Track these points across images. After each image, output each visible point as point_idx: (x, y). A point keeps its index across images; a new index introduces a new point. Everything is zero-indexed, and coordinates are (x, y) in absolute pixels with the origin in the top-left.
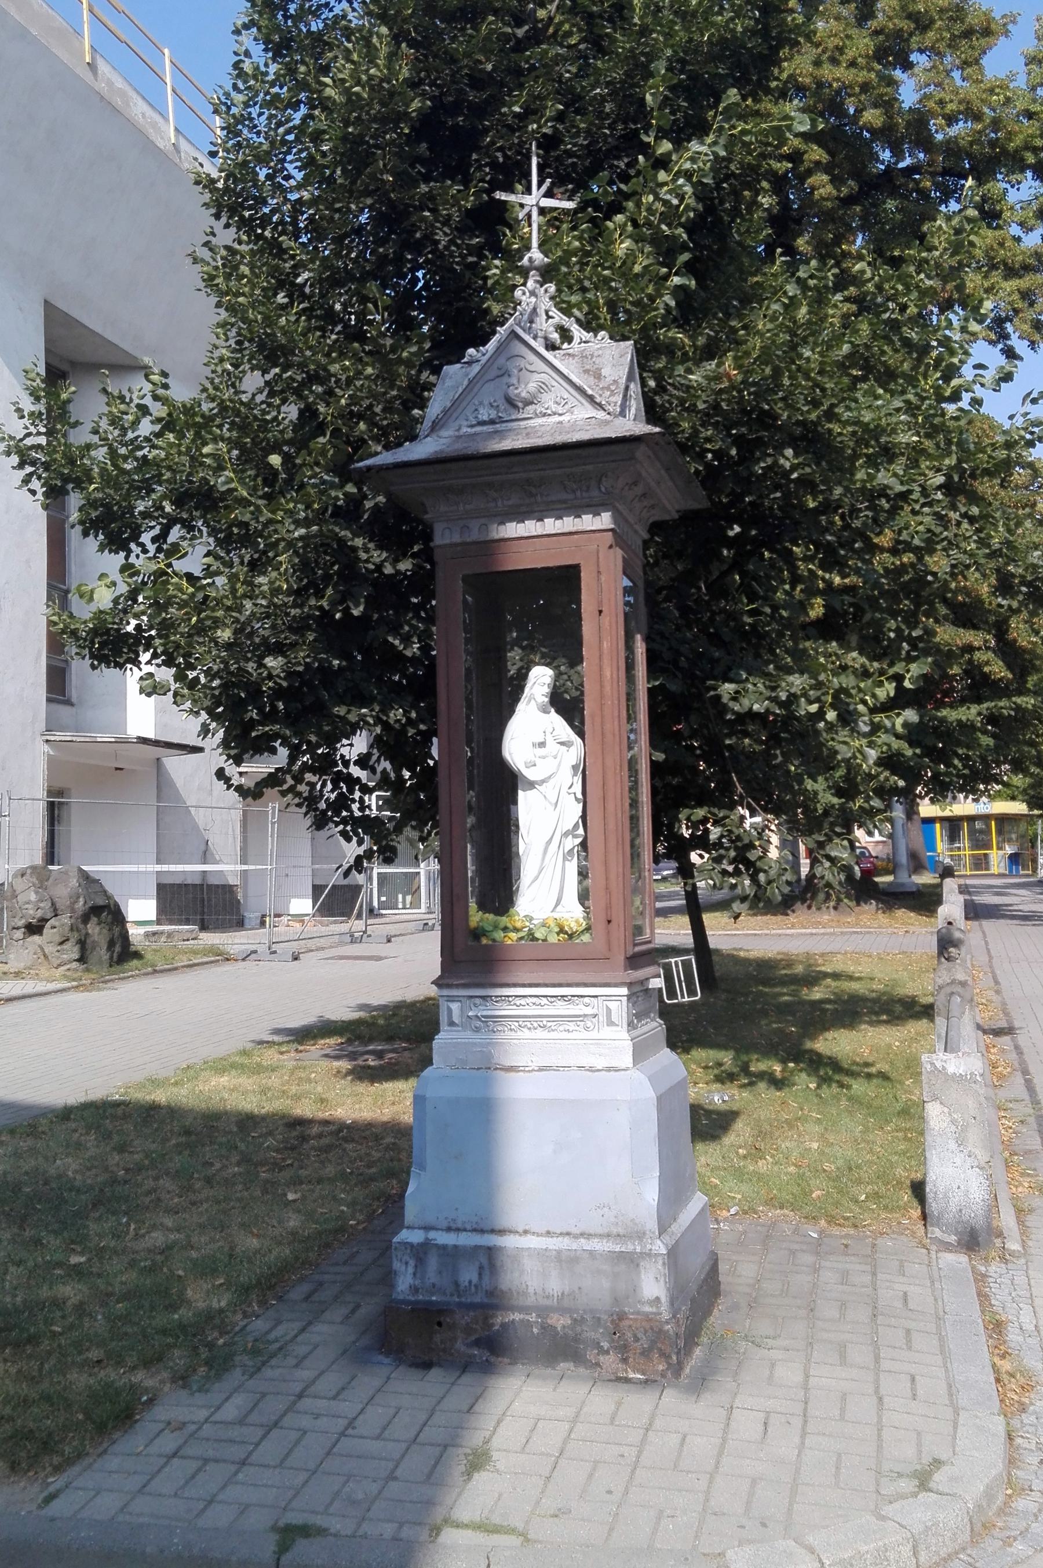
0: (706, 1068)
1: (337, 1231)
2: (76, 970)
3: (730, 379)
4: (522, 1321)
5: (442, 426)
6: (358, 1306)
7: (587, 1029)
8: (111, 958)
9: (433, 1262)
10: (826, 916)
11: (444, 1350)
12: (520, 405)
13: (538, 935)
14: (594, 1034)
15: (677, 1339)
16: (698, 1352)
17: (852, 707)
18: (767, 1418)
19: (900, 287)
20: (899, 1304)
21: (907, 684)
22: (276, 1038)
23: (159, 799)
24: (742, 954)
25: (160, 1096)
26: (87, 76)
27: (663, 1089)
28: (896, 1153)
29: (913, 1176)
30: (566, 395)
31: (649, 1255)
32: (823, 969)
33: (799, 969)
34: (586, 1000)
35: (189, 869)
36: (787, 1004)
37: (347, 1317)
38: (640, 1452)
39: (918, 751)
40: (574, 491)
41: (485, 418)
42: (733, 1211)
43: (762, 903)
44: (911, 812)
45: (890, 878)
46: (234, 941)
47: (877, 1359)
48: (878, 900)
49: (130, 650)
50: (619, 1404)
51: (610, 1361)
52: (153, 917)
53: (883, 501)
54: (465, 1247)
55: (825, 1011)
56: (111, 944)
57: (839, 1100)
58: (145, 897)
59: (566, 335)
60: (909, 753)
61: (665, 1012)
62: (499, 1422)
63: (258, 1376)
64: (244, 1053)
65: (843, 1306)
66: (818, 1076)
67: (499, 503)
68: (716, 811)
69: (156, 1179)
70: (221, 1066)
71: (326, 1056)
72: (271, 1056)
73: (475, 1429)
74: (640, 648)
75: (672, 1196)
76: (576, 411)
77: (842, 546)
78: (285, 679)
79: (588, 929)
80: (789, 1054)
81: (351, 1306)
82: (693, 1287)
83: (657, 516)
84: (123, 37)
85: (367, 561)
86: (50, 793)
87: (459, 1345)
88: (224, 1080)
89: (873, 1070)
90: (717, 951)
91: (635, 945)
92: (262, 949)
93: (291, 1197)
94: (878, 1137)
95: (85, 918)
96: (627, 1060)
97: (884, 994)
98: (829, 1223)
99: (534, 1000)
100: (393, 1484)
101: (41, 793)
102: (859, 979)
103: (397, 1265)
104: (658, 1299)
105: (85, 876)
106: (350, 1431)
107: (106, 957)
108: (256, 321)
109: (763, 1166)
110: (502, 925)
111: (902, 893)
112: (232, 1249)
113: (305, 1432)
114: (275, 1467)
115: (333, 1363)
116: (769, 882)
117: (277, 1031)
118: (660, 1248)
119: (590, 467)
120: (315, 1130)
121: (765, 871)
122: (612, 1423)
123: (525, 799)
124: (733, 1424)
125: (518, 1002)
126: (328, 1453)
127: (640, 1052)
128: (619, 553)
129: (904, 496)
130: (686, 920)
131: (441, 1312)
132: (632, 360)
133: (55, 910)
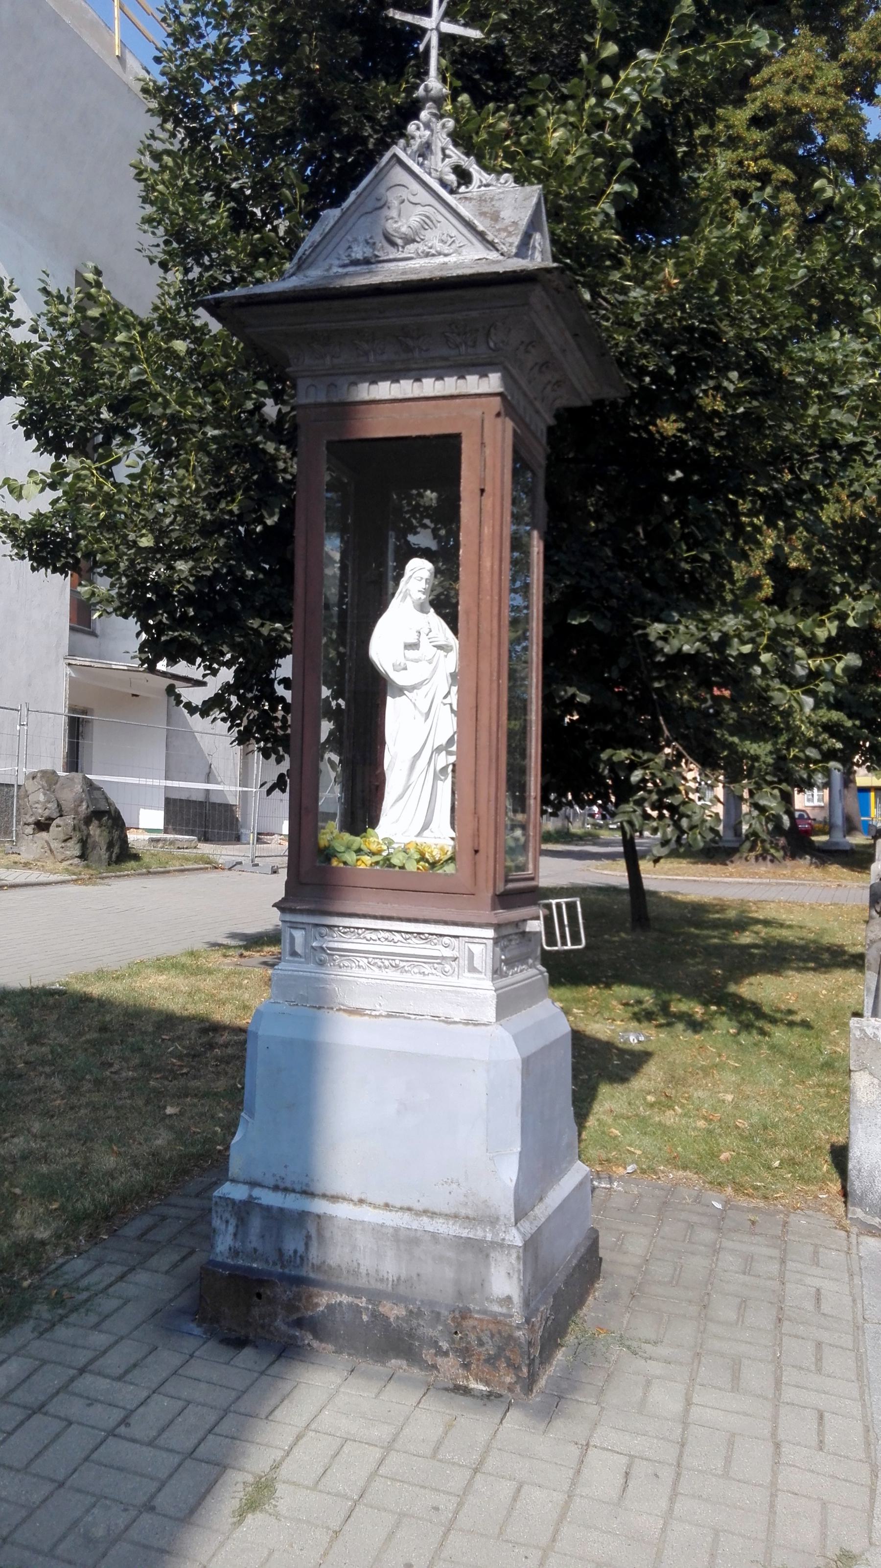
0: (626, 1004)
1: (201, 1156)
2: (77, 865)
3: (670, 287)
4: (350, 1305)
5: (308, 267)
6: (192, 1252)
7: (445, 973)
8: (110, 857)
9: (256, 1223)
10: (763, 868)
11: (263, 1326)
12: (400, 242)
13: (395, 861)
14: (453, 980)
15: (536, 1339)
16: (560, 1356)
17: (788, 650)
18: (630, 1466)
19: (862, 208)
20: (809, 1305)
21: (851, 622)
22: (233, 943)
23: (168, 724)
24: (680, 897)
25: (96, 990)
26: (117, 68)
27: (533, 1047)
28: (817, 1111)
29: (834, 1139)
30: (454, 233)
31: (501, 1245)
32: (755, 915)
33: (732, 914)
34: (446, 940)
35: (194, 787)
36: (716, 947)
37: (175, 1266)
38: (460, 1505)
39: (857, 723)
40: (457, 346)
41: (359, 256)
42: (630, 1169)
43: (681, 849)
44: (848, 779)
45: (824, 838)
46: (223, 853)
47: (778, 1383)
48: (812, 856)
49: (68, 555)
50: (449, 1427)
51: (449, 1365)
52: (161, 826)
53: (835, 453)
54: (291, 1211)
55: (752, 956)
56: (110, 846)
57: (760, 1048)
58: (158, 809)
59: (464, 176)
60: (849, 724)
61: (547, 959)
62: (299, 1438)
63: (47, 1335)
64: (192, 954)
65: (743, 1304)
66: (740, 1022)
67: (372, 357)
68: (640, 753)
69: (48, 1076)
70: (161, 965)
71: (265, 963)
72: (215, 959)
73: (268, 1446)
74: (537, 547)
75: (538, 1170)
76: (464, 251)
77: (789, 496)
78: (194, 583)
79: (452, 859)
80: (712, 997)
81: (185, 1251)
82: (560, 1278)
83: (565, 400)
84: (151, 37)
85: (285, 471)
86: (72, 709)
87: (278, 1323)
88: (162, 978)
89: (797, 1018)
90: (654, 894)
91: (507, 881)
92: (246, 861)
93: (169, 1110)
94: (799, 1092)
95: (88, 821)
96: (490, 1014)
97: (814, 942)
98: (736, 1191)
99: (387, 935)
100: (146, 1519)
101: (62, 708)
102: (790, 927)
103: (217, 1223)
104: (509, 1299)
105: (91, 786)
106: (122, 1430)
107: (105, 856)
108: (177, 214)
109: (670, 1118)
110: (355, 847)
111: (837, 851)
112: (86, 1166)
113: (70, 1423)
114: (18, 1471)
115: (136, 1328)
116: (692, 828)
117: (233, 936)
118: (515, 1238)
119: (474, 314)
120: (225, 1037)
121: (688, 817)
122: (434, 1456)
123: (393, 707)
124: (585, 1471)
125: (368, 935)
126: (87, 1459)
127: (507, 1005)
128: (510, 424)
129: (856, 448)
130: (622, 864)
131: (261, 1282)
132: (538, 204)
133: (61, 811)
